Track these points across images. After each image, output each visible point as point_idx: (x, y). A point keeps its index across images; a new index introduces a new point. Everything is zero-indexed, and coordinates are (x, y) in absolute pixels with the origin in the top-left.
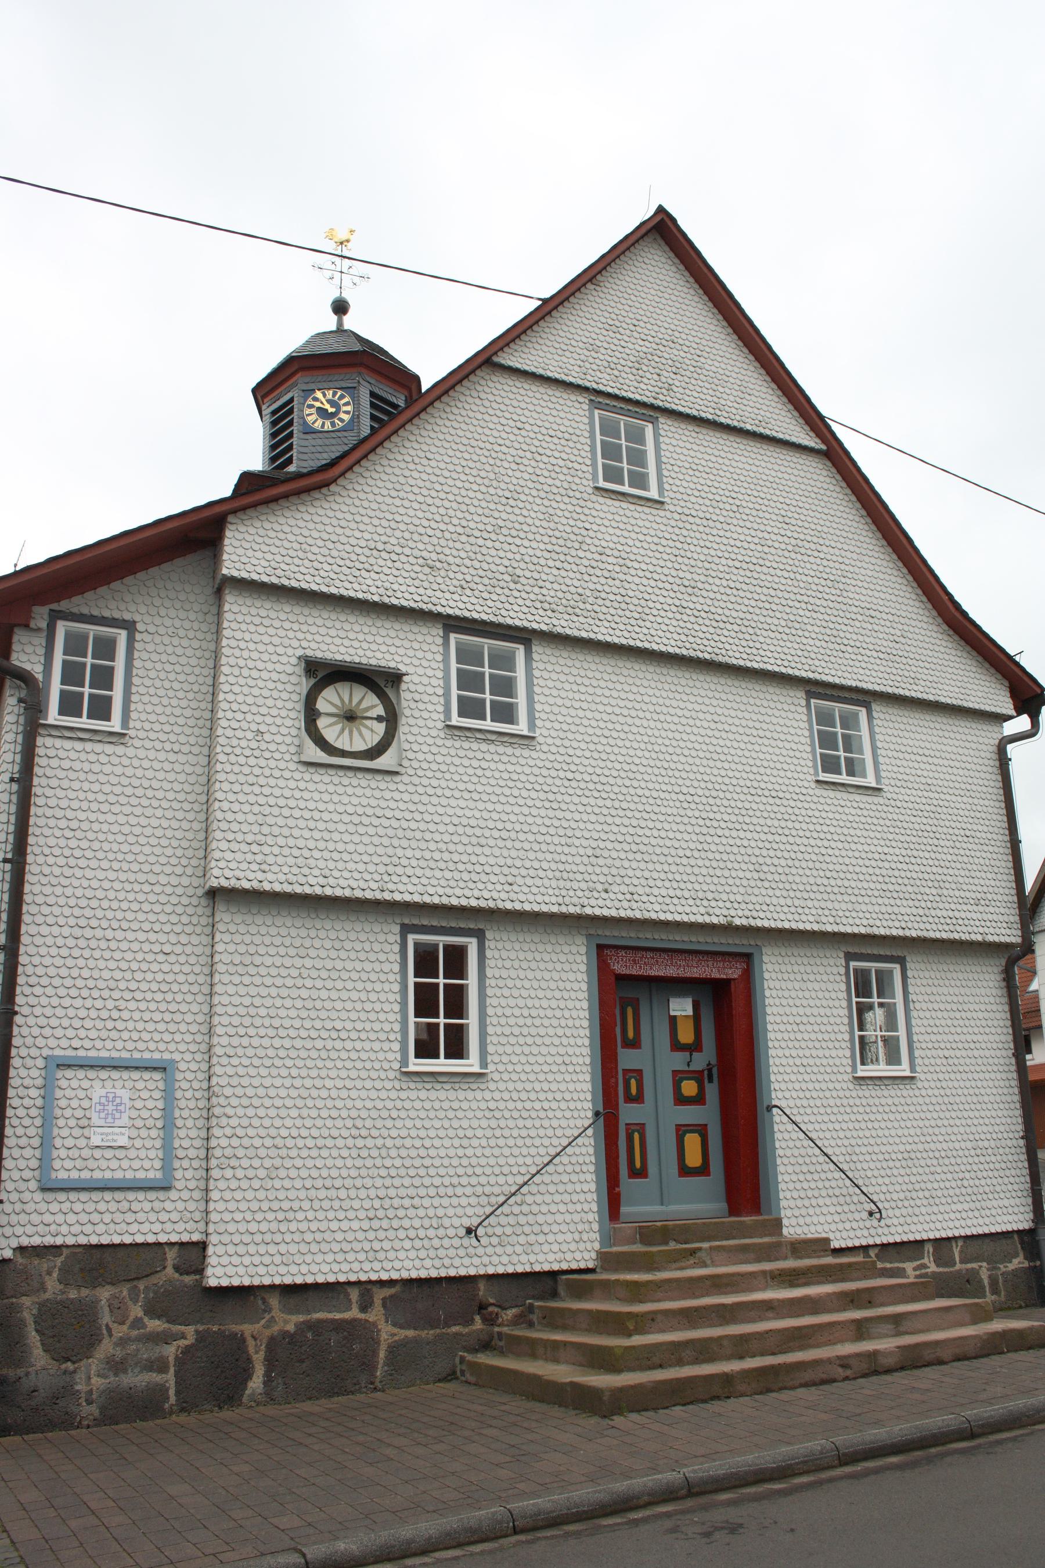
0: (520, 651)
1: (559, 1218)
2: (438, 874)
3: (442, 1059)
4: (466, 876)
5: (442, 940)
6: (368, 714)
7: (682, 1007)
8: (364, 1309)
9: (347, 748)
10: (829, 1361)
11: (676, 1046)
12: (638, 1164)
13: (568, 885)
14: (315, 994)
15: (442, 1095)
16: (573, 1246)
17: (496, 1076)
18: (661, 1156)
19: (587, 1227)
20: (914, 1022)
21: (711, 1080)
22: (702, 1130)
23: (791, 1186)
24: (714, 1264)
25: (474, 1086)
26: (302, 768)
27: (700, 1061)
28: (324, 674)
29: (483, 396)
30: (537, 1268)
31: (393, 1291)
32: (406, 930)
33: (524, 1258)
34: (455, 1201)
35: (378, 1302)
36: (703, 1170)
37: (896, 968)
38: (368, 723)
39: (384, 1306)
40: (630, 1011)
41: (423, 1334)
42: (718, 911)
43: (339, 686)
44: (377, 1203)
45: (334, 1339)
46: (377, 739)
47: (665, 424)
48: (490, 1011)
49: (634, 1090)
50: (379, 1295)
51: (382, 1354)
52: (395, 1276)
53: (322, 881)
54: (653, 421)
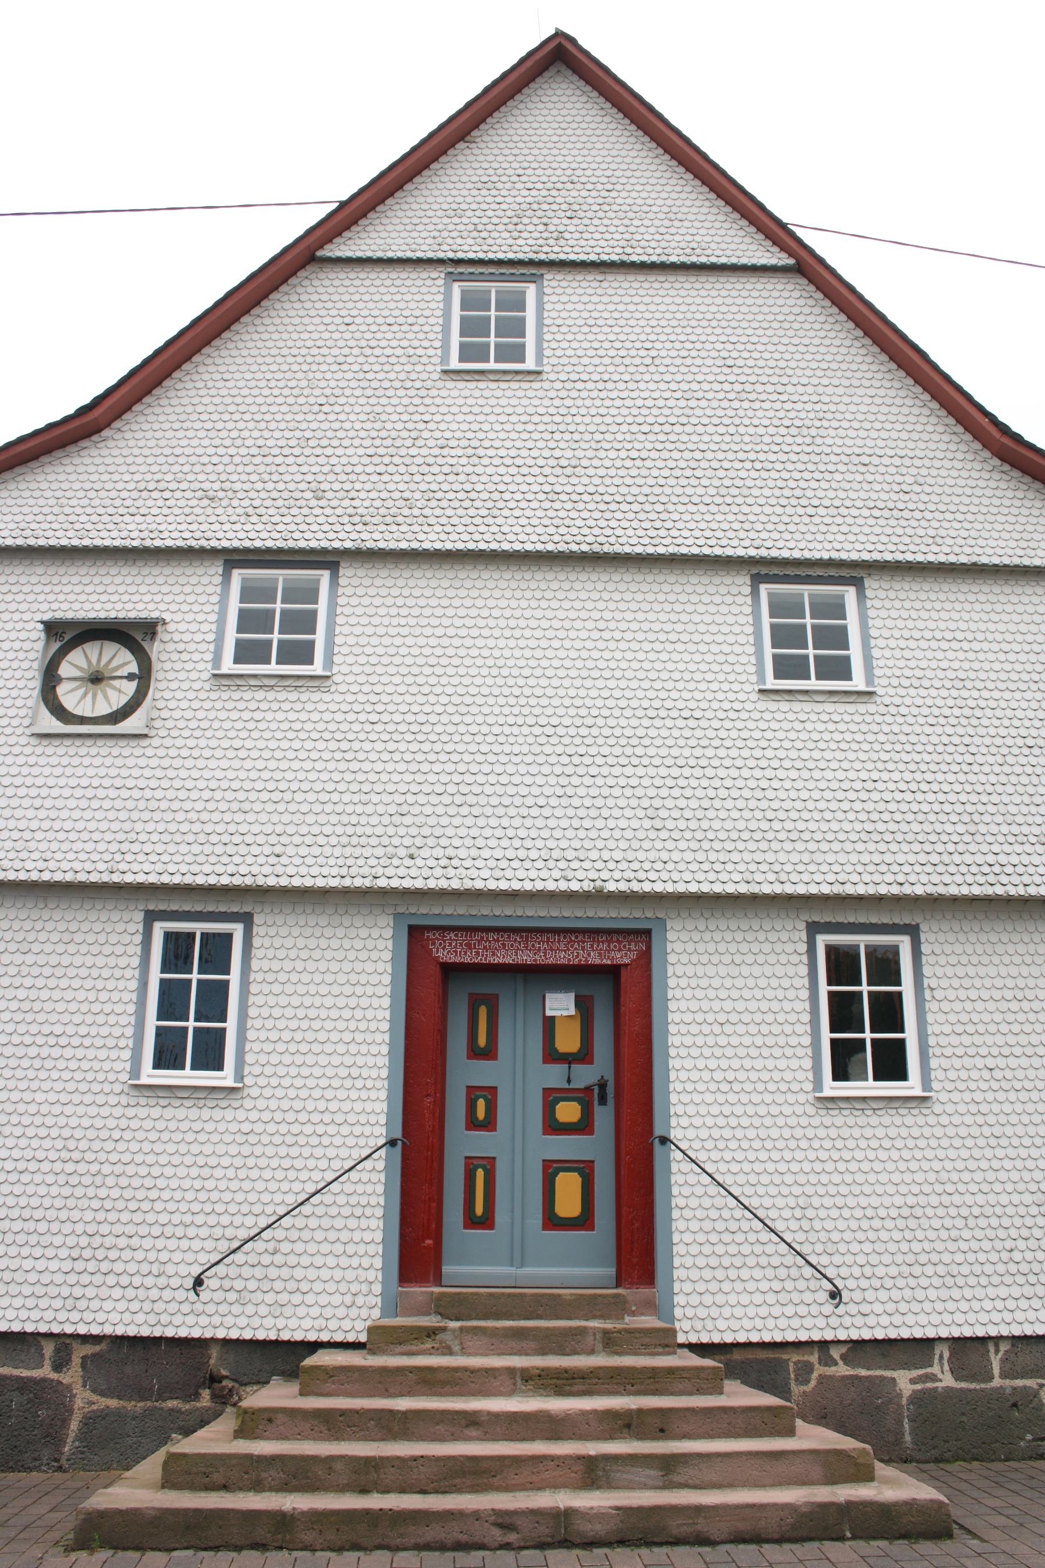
0: (850, 594)
1: (325, 1274)
2: (184, 848)
3: (188, 1071)
4: (219, 849)
5: (862, 941)
6: (119, 673)
7: (561, 1005)
8: (57, 1367)
9: (88, 714)
10: (476, 1515)
11: (551, 1055)
12: (479, 1210)
13: (358, 851)
14: (33, 994)
15: (181, 1113)
16: (341, 1312)
17: (255, 1092)
18: (517, 1198)
19: (364, 1288)
20: (930, 1018)
21: (603, 1101)
22: (586, 1170)
23: (694, 1249)
24: (464, 1351)
25: (224, 1103)
26: (34, 741)
27: (585, 1076)
28: (67, 634)
29: (303, 298)
30: (285, 1336)
31: (97, 1348)
32: (814, 929)
33: (269, 1322)
34: (185, 1244)
35: (76, 1360)
36: (585, 1221)
37: (904, 944)
38: (116, 683)
39: (83, 1365)
40: (483, 1012)
41: (130, 1405)
42: (581, 875)
43: (87, 646)
44: (84, 1241)
45: (16, 1400)
46: (124, 700)
47: (552, 280)
48: (252, 1012)
49: (481, 1113)
50: (80, 1352)
51: (74, 1425)
52: (95, 1330)
53: (41, 865)
54: (534, 279)
